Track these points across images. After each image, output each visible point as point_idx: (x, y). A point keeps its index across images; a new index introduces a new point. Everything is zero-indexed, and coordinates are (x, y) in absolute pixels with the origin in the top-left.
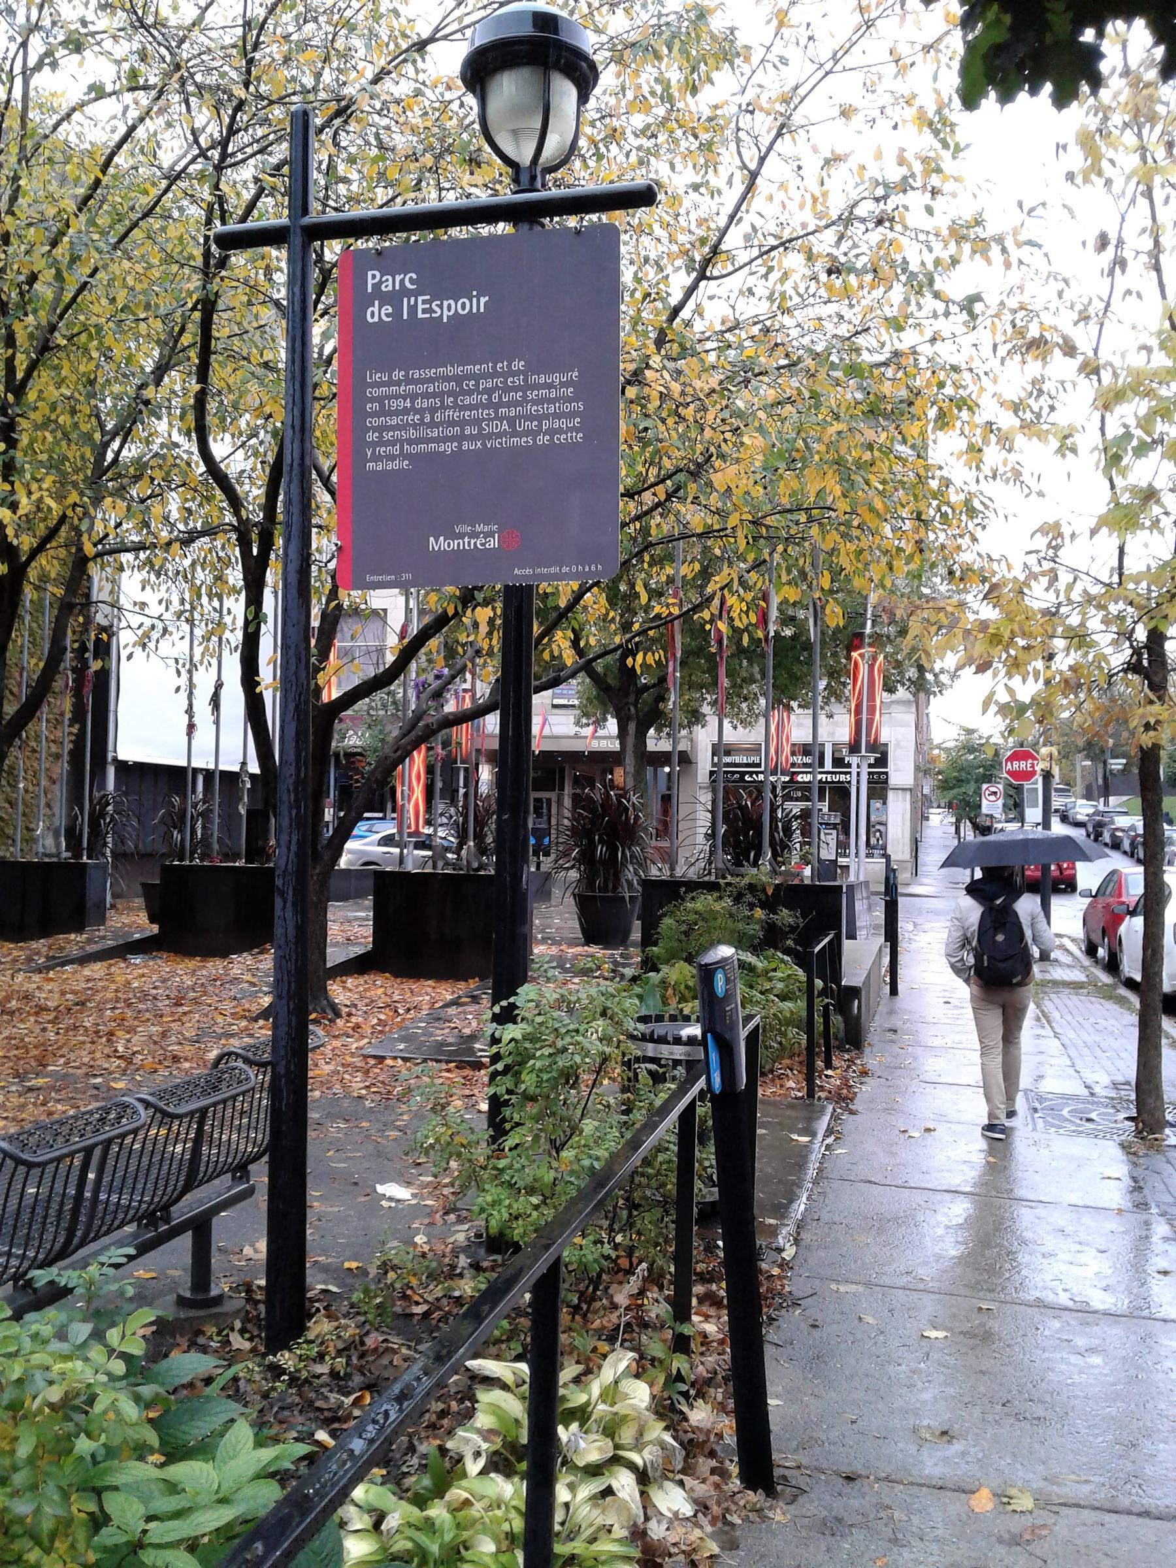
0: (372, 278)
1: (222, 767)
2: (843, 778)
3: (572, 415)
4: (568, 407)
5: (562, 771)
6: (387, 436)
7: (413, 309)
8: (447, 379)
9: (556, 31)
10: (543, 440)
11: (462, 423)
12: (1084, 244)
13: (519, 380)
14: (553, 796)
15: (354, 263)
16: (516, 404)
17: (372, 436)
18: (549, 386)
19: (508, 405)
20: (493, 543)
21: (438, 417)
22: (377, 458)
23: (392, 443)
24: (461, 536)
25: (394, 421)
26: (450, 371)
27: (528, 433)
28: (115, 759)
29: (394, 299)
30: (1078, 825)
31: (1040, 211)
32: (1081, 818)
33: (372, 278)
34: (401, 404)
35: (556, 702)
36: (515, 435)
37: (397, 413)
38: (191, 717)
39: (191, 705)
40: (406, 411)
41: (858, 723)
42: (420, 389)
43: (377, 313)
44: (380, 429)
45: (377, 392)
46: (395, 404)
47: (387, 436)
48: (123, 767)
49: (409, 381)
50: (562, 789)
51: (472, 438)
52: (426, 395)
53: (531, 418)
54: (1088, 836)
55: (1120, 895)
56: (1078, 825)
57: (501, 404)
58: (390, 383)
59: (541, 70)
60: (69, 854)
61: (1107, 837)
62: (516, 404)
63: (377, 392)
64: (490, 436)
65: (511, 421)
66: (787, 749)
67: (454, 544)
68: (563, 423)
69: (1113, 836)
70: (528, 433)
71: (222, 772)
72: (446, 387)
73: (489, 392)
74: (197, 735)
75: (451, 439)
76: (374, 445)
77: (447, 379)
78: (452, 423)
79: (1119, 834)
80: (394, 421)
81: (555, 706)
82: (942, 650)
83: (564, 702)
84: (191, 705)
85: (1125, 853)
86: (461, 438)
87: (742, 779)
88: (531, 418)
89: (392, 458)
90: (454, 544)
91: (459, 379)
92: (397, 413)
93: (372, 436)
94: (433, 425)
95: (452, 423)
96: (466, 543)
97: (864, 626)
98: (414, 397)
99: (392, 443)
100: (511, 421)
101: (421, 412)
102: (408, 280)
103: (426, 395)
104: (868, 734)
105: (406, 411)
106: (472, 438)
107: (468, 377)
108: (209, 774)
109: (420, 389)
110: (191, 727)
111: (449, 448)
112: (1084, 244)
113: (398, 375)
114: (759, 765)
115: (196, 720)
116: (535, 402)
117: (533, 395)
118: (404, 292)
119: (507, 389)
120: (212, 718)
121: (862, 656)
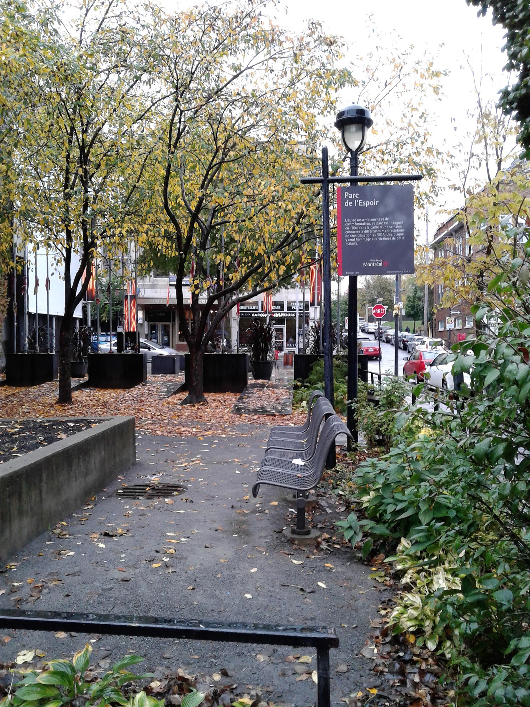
0: (346, 194)
1: (39, 312)
2: (291, 315)
3: (402, 232)
4: (400, 231)
6: (351, 236)
7: (358, 203)
8: (367, 222)
9: (364, 114)
10: (394, 238)
11: (372, 234)
13: (387, 223)
14: (170, 324)
15: (341, 191)
16: (386, 229)
17: (347, 236)
18: (395, 225)
19: (384, 229)
20: (381, 264)
21: (365, 232)
22: (348, 242)
23: (353, 238)
24: (372, 262)
25: (353, 232)
26: (368, 220)
27: (389, 237)
28: (28, 312)
29: (353, 200)
30: (370, 333)
31: (468, 157)
32: (373, 330)
33: (346, 194)
34: (353, 228)
35: (171, 283)
36: (386, 237)
37: (354, 230)
40: (356, 230)
41: (314, 294)
42: (360, 224)
43: (347, 204)
44: (349, 234)
45: (348, 224)
46: (353, 228)
47: (351, 236)
49: (357, 222)
51: (374, 237)
52: (362, 226)
53: (390, 233)
54: (376, 338)
55: (421, 359)
56: (370, 333)
57: (382, 229)
58: (352, 222)
59: (361, 125)
61: (384, 338)
62: (386, 229)
63: (348, 224)
64: (379, 237)
65: (385, 234)
66: (271, 303)
67: (370, 265)
68: (399, 235)
69: (387, 338)
70: (389, 237)
71: (39, 314)
72: (367, 224)
73: (379, 226)
75: (369, 237)
76: (348, 238)
77: (367, 222)
78: (369, 233)
79: (389, 337)
80: (353, 232)
85: (392, 344)
86: (372, 237)
87: (251, 316)
88: (390, 233)
89: (353, 242)
90: (370, 265)
91: (371, 222)
92: (354, 230)
93: (347, 236)
94: (364, 234)
95: (369, 233)
96: (373, 264)
97: (315, 255)
98: (358, 226)
99: (353, 238)
100: (385, 234)
101: (361, 230)
102: (357, 195)
103: (362, 226)
104: (318, 299)
105: (356, 230)
106: (374, 237)
107: (374, 221)
109: (360, 224)
111: (369, 240)
113: (354, 220)
114: (258, 310)
116: (391, 229)
117: (391, 227)
118: (355, 198)
119: (384, 225)
121: (315, 267)
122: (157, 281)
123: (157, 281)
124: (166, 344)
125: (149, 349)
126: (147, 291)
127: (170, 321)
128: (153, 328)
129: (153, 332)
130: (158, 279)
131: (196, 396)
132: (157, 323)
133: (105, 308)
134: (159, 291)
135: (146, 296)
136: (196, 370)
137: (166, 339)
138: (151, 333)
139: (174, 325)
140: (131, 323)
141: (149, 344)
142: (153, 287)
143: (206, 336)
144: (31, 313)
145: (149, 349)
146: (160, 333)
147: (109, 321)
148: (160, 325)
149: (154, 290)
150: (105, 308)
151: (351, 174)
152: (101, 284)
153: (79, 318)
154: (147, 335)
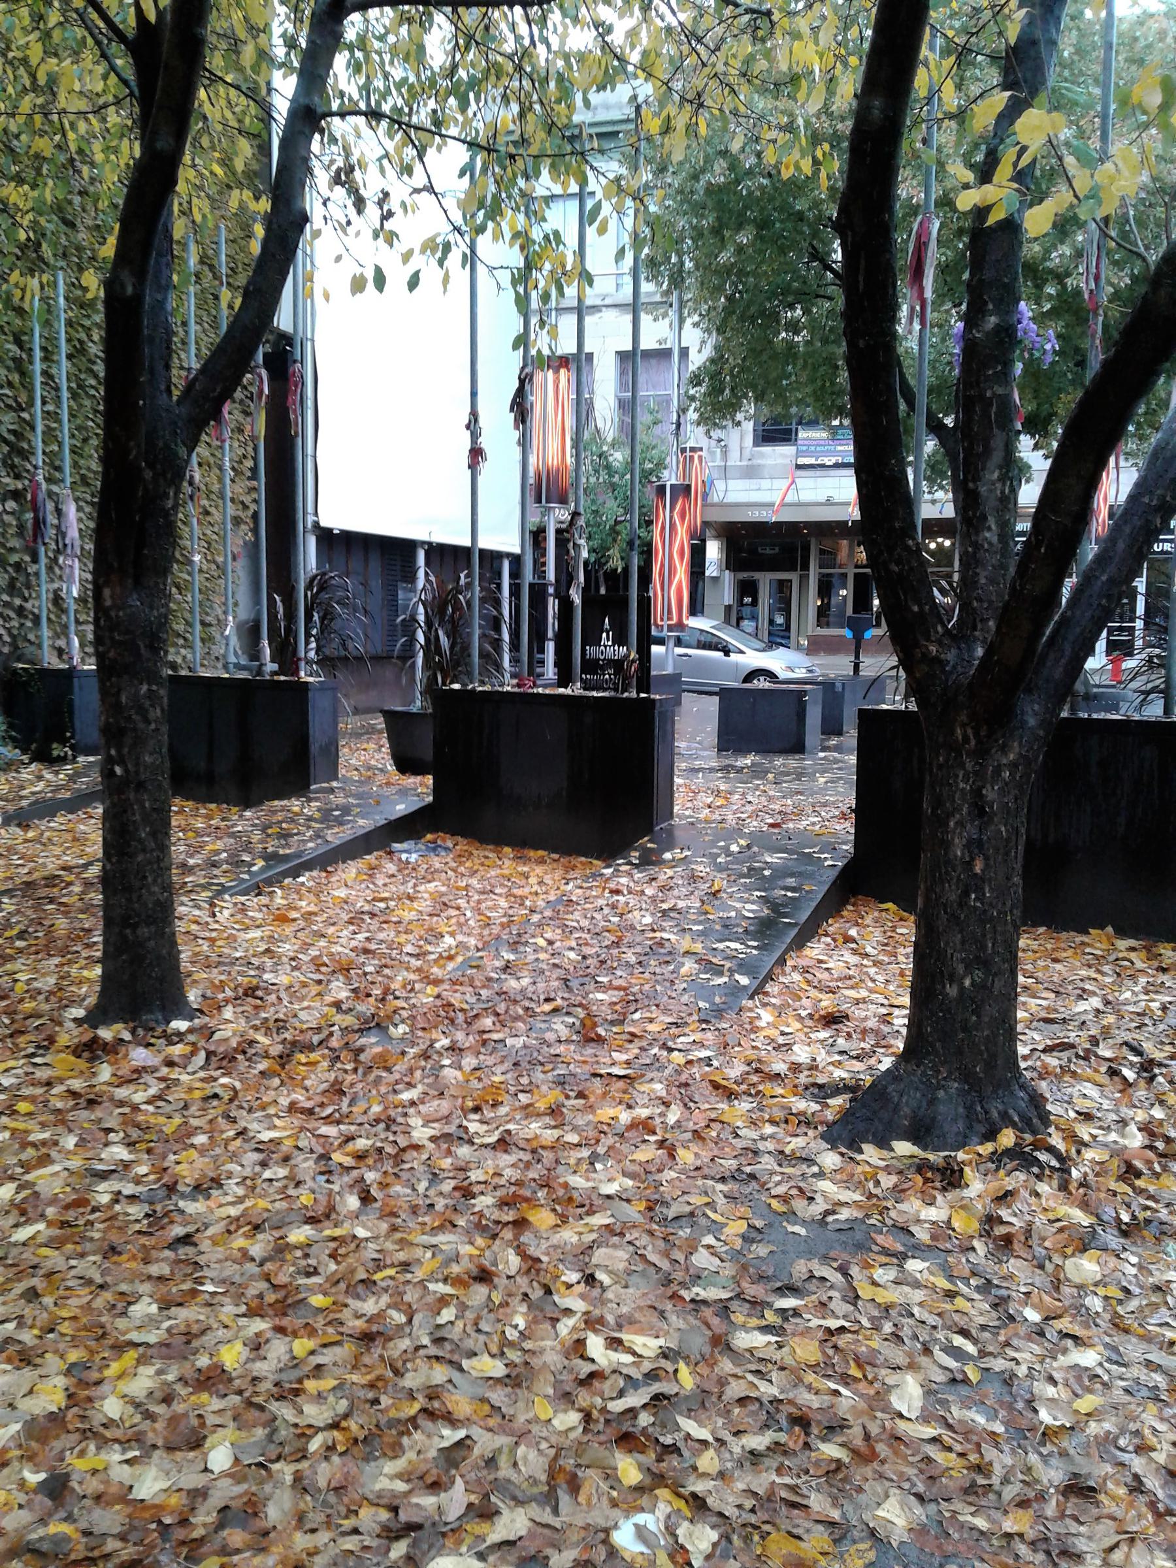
5: (806, 549)
12: (327, 297)
14: (794, 577)
28: (316, 525)
35: (801, 461)
38: (475, 436)
39: (474, 414)
48: (326, 537)
50: (805, 567)
60: (275, 667)
74: (486, 469)
81: (799, 467)
82: (935, 453)
83: (811, 461)
84: (474, 414)
108: (442, 555)
110: (476, 453)
112: (327, 297)
115: (484, 442)
120: (516, 435)
122: (762, 455)
123: (762, 455)
124: (778, 638)
125: (727, 653)
126: (732, 484)
127: (793, 568)
128: (747, 589)
129: (748, 600)
130: (767, 450)
131: (967, 1076)
132: (757, 575)
133: (618, 533)
134: (765, 483)
135: (732, 498)
136: (975, 883)
137: (780, 620)
138: (741, 604)
139: (804, 579)
140: (672, 571)
141: (727, 636)
142: (751, 472)
143: (1077, 592)
144: (329, 531)
145: (727, 653)
146: (765, 600)
147: (626, 570)
148: (765, 580)
149: (753, 483)
150: (618, 533)
151: (926, 522)
152: (608, 467)
153: (508, 555)
154: (728, 608)
